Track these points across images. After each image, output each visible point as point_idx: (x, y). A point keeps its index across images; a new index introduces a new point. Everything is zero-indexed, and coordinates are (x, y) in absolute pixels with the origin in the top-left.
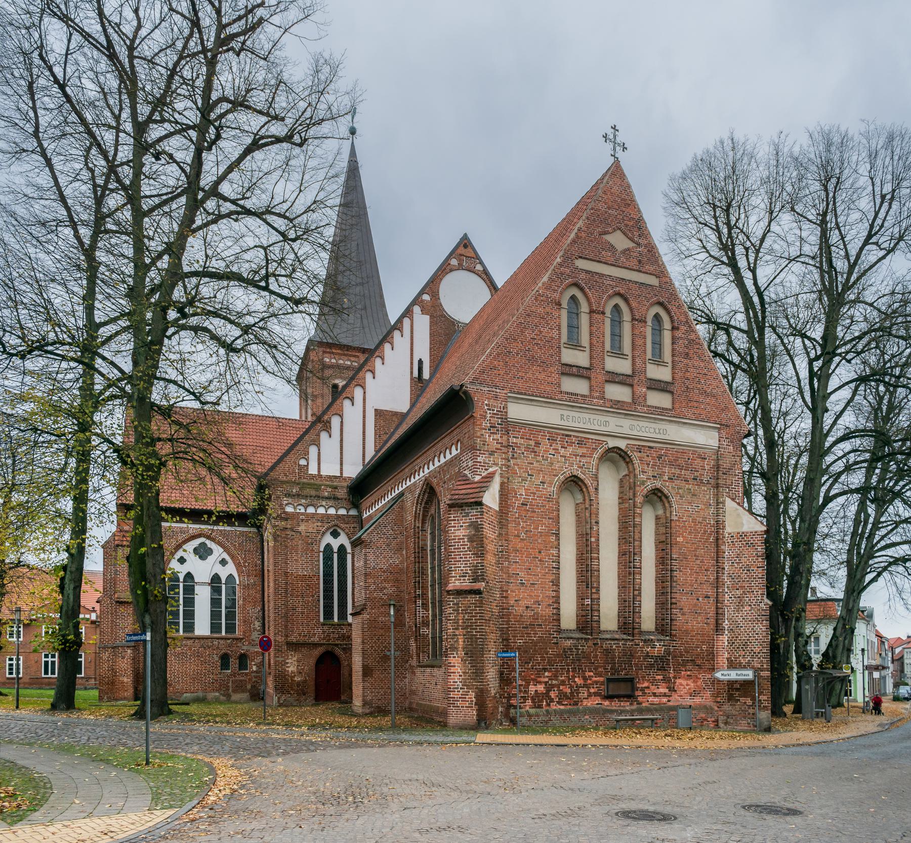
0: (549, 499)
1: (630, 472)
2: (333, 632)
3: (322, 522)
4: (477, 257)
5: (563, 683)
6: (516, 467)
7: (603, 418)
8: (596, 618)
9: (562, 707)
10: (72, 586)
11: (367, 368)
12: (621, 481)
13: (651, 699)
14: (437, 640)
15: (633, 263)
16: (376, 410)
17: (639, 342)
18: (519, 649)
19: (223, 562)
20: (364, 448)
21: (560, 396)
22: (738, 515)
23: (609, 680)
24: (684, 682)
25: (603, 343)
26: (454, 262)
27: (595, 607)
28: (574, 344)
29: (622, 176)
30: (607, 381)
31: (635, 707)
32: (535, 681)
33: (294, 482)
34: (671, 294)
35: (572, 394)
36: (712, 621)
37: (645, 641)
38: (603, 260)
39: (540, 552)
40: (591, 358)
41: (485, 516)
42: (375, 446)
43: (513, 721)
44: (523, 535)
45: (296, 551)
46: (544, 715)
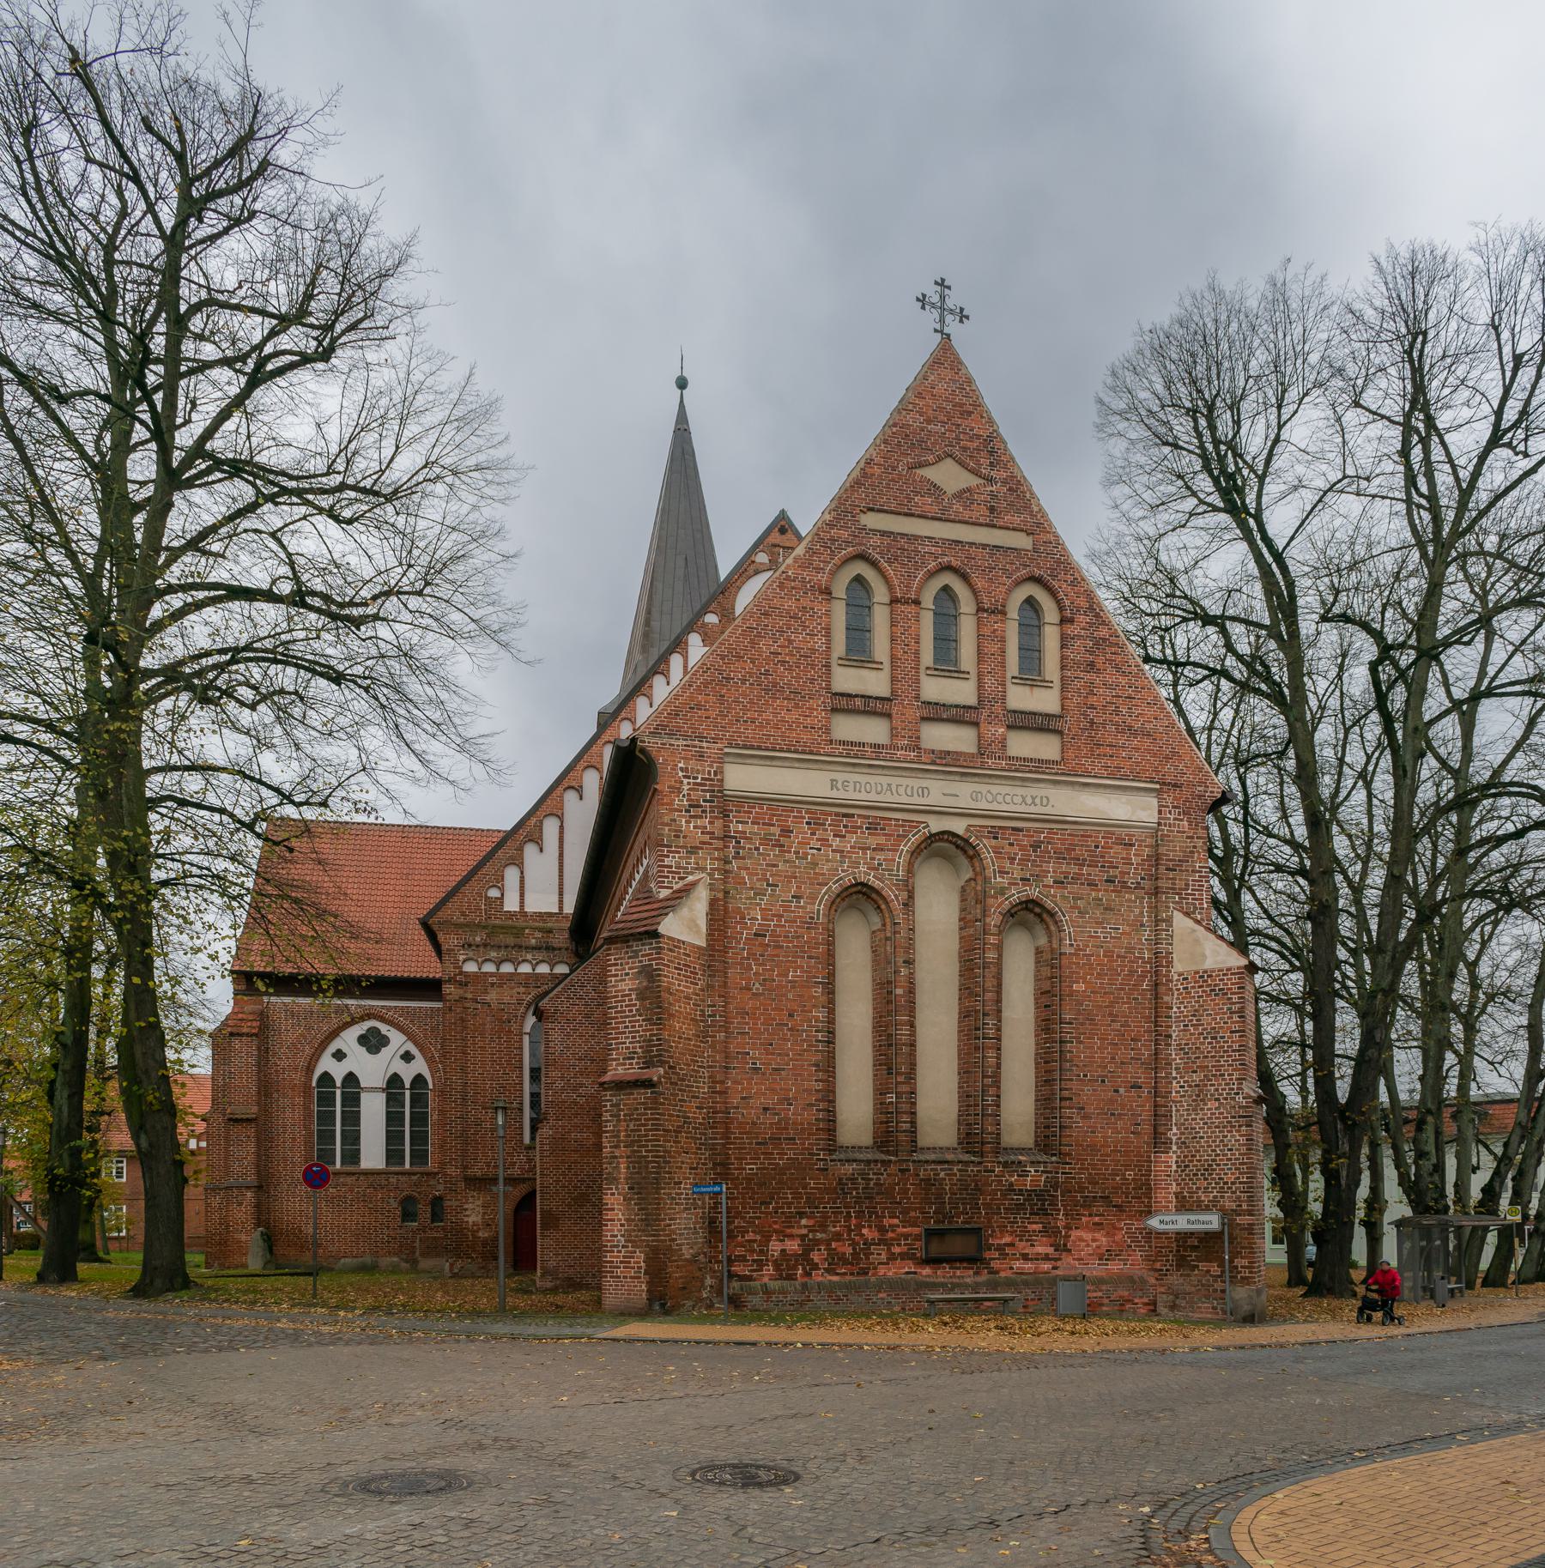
3: (527, 986)
5: (837, 1237)
6: (744, 873)
7: (916, 783)
9: (835, 1278)
10: (65, 1094)
13: (1017, 1265)
15: (980, 513)
19: (407, 1057)
21: (828, 749)
22: (1197, 941)
23: (930, 1233)
24: (1087, 1236)
25: (917, 653)
28: (859, 654)
29: (956, 364)
30: (923, 719)
31: (984, 1277)
32: (784, 1236)
33: (478, 925)
34: (1059, 562)
36: (1147, 1128)
37: (1005, 1165)
39: (791, 1015)
40: (893, 679)
41: (667, 956)
43: (735, 1302)
44: (757, 987)
45: (482, 1034)
46: (796, 1292)
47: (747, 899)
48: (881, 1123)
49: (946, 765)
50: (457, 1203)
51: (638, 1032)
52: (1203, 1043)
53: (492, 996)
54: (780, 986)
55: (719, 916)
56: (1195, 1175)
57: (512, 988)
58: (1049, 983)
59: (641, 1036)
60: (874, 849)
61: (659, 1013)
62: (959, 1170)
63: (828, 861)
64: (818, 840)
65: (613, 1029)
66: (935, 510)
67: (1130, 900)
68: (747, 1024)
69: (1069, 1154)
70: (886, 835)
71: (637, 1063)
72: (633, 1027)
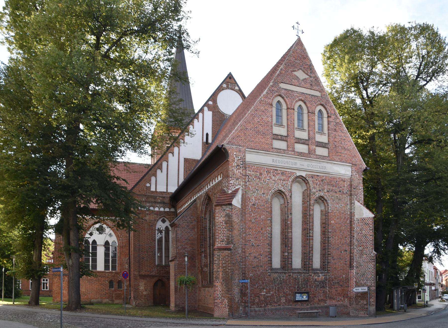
0: (267, 202)
1: (307, 188)
2: (162, 270)
3: (157, 215)
4: (236, 83)
6: (250, 186)
8: (290, 262)
12: (303, 193)
14: (211, 273)
15: (308, 85)
16: (185, 159)
17: (311, 123)
18: (251, 278)
19: (110, 235)
20: (178, 177)
22: (361, 209)
25: (294, 124)
26: (224, 86)
27: (290, 257)
28: (280, 125)
30: (295, 143)
34: (327, 100)
35: (278, 149)
36: (348, 263)
38: (293, 83)
39: (262, 229)
41: (234, 211)
42: (184, 176)
47: (251, 194)
48: (283, 261)
49: (301, 156)
50: (137, 283)
51: (225, 234)
52: (363, 239)
53: (147, 218)
54: (259, 220)
55: (244, 199)
56: (360, 276)
57: (153, 215)
58: (325, 221)
59: (226, 235)
60: (283, 180)
61: (232, 228)
62: (303, 275)
63: (271, 183)
64: (269, 177)
65: (217, 232)
66: (297, 84)
67: (344, 197)
68: (251, 231)
69: (330, 270)
70: (286, 176)
71: (225, 243)
72: (223, 232)
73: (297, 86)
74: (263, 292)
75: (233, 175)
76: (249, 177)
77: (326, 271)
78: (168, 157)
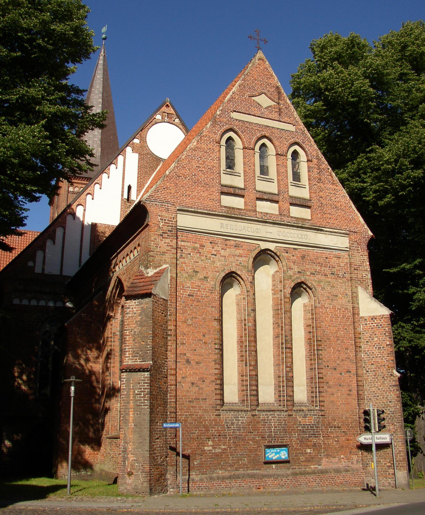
11: (87, 191)
17: (282, 170)
25: (254, 170)
39: (204, 336)
64: (215, 251)
66: (258, 113)
70: (243, 249)
73: (258, 116)
74: (208, 446)
75: (157, 247)
76: (182, 251)
77: (316, 406)
78: (66, 220)
